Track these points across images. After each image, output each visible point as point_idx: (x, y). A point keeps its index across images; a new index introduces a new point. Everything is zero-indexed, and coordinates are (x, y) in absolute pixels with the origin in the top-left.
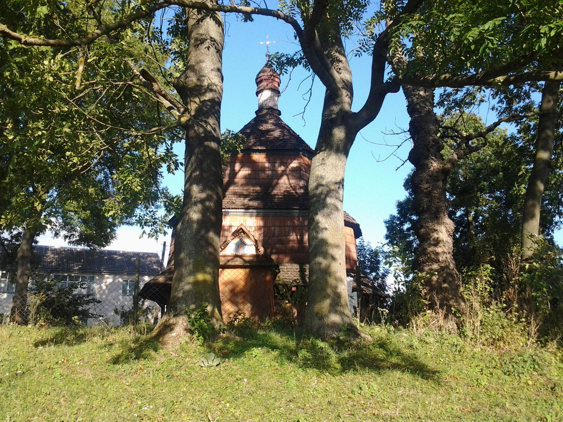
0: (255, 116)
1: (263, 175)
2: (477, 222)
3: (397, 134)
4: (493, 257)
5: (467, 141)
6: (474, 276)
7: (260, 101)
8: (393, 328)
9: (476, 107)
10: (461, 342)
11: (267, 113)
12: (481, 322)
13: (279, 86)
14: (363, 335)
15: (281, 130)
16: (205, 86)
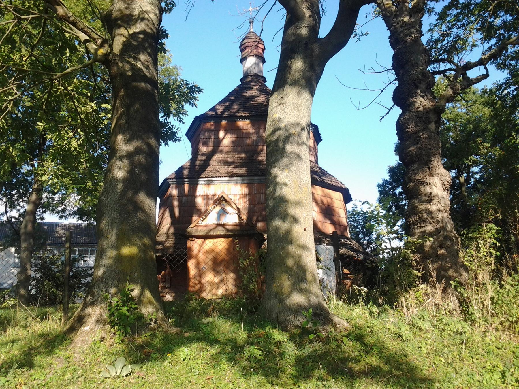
0: (240, 83)
1: (248, 141)
2: (470, 183)
3: (379, 73)
4: (498, 215)
5: (464, 72)
6: (476, 239)
7: (245, 68)
8: (376, 309)
9: (468, 52)
10: (467, 327)
11: (252, 80)
12: (492, 298)
13: (263, 52)
14: (336, 319)
15: (265, 95)
16: (136, 15)
